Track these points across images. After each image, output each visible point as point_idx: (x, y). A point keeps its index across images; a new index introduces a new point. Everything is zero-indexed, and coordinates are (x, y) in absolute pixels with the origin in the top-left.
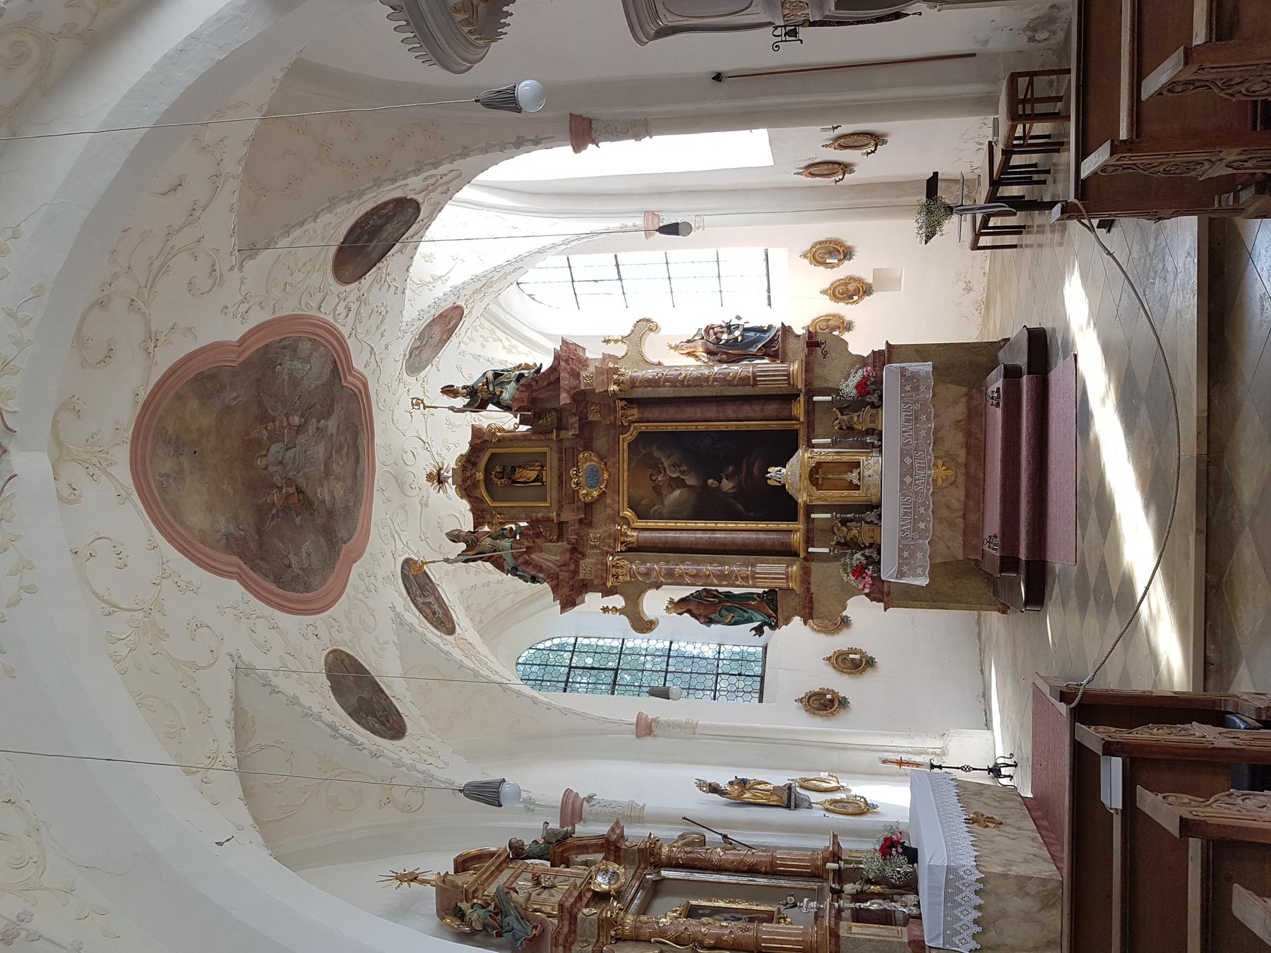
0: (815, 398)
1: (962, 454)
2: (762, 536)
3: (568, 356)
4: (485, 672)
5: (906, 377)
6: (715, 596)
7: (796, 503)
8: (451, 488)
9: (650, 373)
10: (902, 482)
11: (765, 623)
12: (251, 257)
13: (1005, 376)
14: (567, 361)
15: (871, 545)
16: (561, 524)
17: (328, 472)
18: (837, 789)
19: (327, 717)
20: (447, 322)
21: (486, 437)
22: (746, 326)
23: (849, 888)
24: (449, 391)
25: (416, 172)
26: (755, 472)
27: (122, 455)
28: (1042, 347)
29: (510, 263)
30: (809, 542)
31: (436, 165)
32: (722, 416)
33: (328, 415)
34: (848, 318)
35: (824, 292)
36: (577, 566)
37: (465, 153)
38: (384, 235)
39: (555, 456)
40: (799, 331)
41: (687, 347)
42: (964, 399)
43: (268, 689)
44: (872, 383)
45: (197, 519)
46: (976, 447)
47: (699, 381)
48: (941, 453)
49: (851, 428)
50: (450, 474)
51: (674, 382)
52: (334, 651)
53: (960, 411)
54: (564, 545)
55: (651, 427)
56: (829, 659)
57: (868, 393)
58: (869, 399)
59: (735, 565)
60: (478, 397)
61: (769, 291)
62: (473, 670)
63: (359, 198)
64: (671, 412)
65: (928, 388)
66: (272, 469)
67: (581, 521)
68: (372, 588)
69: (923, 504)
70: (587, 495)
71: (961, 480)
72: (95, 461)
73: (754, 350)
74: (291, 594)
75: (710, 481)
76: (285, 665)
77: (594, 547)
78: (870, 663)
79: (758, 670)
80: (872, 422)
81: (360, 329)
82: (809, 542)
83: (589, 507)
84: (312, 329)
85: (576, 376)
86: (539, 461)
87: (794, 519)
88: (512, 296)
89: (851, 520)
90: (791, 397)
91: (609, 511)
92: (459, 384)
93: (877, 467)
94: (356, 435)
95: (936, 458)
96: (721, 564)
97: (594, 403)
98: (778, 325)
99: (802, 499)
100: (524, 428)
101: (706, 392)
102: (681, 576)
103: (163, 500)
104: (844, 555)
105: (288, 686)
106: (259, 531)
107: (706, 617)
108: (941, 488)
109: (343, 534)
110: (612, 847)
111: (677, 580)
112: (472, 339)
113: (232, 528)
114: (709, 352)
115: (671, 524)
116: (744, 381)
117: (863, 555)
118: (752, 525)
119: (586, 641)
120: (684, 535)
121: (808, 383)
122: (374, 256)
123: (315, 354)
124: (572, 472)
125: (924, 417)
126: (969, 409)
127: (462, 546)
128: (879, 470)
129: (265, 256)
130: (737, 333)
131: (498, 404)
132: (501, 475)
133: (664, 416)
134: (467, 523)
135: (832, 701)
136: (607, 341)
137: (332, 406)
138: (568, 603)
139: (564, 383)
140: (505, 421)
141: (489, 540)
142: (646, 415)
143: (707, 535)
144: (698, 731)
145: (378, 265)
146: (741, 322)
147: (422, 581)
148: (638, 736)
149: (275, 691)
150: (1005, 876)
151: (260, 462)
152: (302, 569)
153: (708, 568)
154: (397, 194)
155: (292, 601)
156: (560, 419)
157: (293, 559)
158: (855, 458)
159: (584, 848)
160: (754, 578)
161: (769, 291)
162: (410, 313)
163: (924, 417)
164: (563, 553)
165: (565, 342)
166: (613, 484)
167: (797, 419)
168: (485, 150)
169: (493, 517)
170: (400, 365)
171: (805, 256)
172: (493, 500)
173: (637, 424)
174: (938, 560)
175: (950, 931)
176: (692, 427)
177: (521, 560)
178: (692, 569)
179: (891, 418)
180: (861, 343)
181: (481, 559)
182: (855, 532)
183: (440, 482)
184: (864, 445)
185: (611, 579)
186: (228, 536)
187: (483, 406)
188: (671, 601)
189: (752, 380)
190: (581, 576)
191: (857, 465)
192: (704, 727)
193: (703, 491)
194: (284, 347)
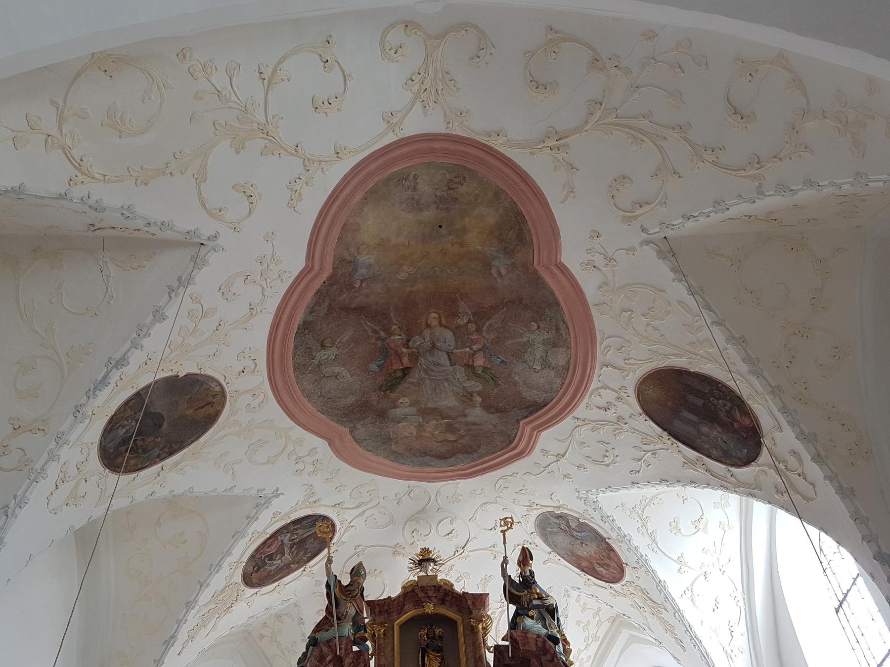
4: (193, 618)
12: (660, 254)
17: (426, 413)
19: (136, 358)
20: (602, 561)
21: (475, 612)
24: (526, 557)
25: (802, 436)
27: (434, 124)
29: (688, 629)
31: (818, 458)
38: (705, 429)
43: (175, 284)
50: (430, 573)
52: (223, 393)
60: (522, 592)
62: (195, 601)
63: (752, 372)
66: (427, 333)
68: (301, 466)
72: (427, 85)
76: (204, 315)
84: (580, 361)
92: (536, 566)
100: (490, 657)
103: (389, 179)
106: (360, 310)
113: (362, 271)
122: (678, 425)
123: (553, 373)
129: (663, 271)
131: (517, 614)
132: (432, 637)
137: (498, 410)
141: (352, 612)
145: (665, 434)
149: (171, 291)
152: (319, 365)
154: (765, 421)
157: (331, 353)
169: (382, 624)
170: (547, 504)
181: (330, 603)
194: (558, 329)
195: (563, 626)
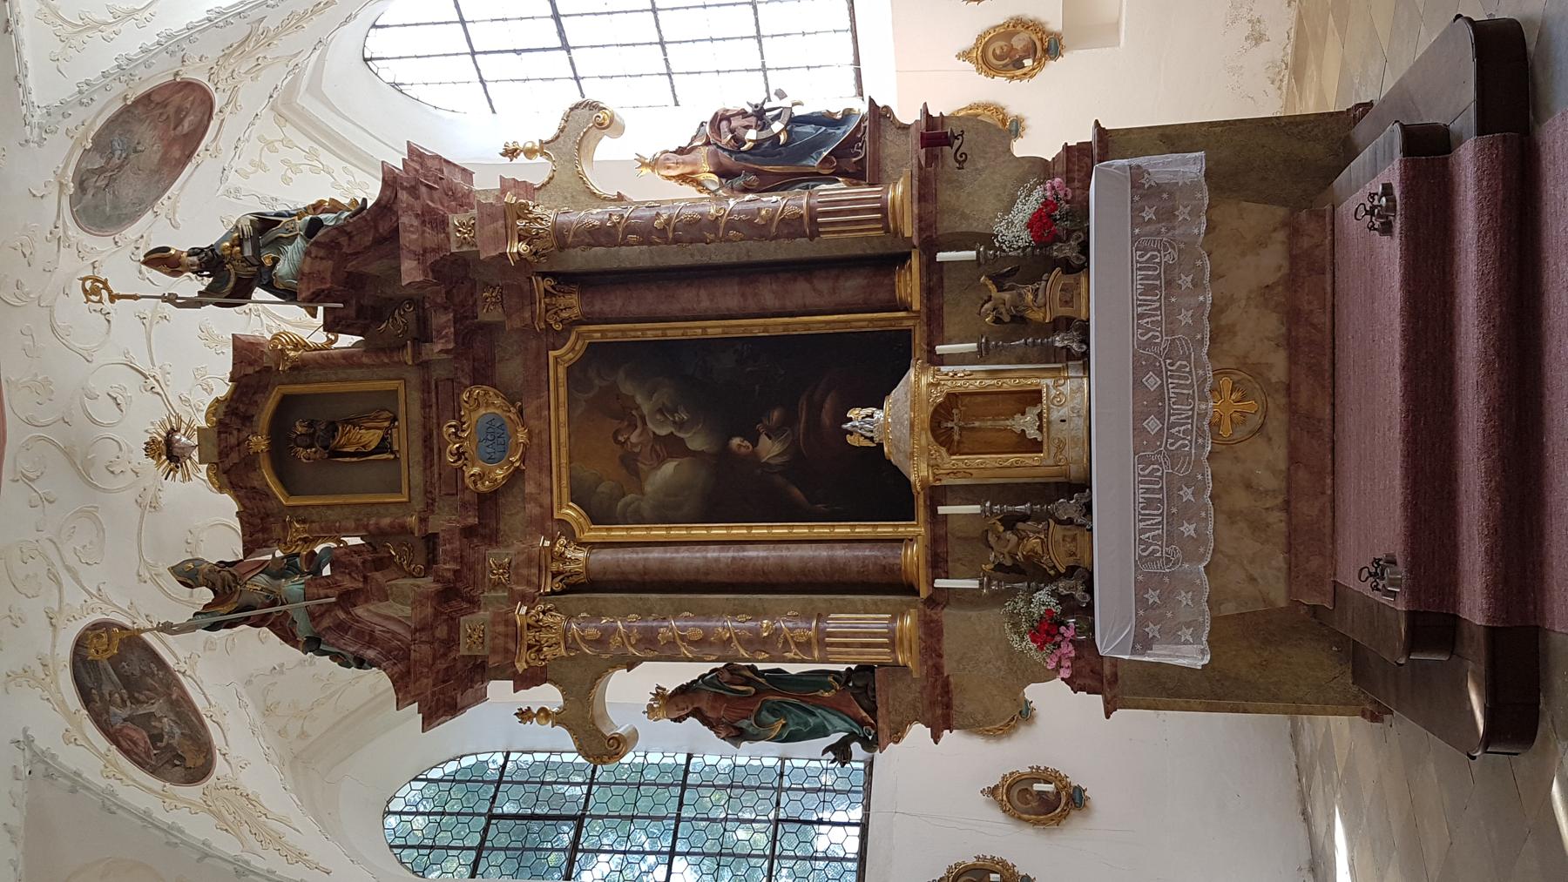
0: (942, 256)
1: (1278, 365)
2: (840, 553)
5: (1143, 190)
6: (748, 682)
9: (595, 215)
10: (1139, 431)
11: (852, 737)
14: (413, 190)
15: (1071, 571)
16: (431, 540)
21: (266, 362)
22: (798, 111)
24: (161, 260)
26: (826, 418)
30: (938, 564)
32: (752, 305)
34: (1013, 110)
35: (965, 55)
36: (454, 629)
39: (416, 396)
40: (908, 114)
42: (1281, 236)
44: (1064, 217)
47: (694, 229)
48: (1229, 363)
49: (1019, 320)
51: (646, 233)
53: (1271, 262)
54: (428, 584)
56: (993, 792)
57: (1056, 238)
58: (1058, 251)
59: (785, 617)
60: (231, 271)
61: (857, 61)
62: (235, 861)
64: (648, 299)
65: (1195, 213)
67: (468, 532)
69: (1189, 481)
70: (481, 476)
71: (1278, 422)
73: (814, 163)
75: (736, 441)
77: (496, 585)
80: (1066, 303)
82: (938, 564)
83: (489, 502)
86: (382, 407)
87: (909, 516)
89: (1024, 518)
90: (889, 262)
91: (532, 509)
92: (180, 244)
93: (1079, 401)
95: (1218, 373)
96: (757, 615)
97: (487, 285)
99: (918, 472)
100: (346, 341)
101: (718, 254)
102: (671, 643)
104: (1013, 593)
107: (731, 725)
108: (1229, 444)
111: (669, 652)
114: (724, 173)
115: (659, 532)
116: (791, 226)
117: (1054, 594)
118: (822, 530)
120: (683, 555)
125: (1186, 281)
126: (1293, 259)
128: (1087, 407)
130: (777, 127)
131: (270, 287)
132: (310, 440)
133: (633, 308)
138: (439, 708)
139: (409, 238)
140: (303, 326)
141: (262, 580)
142: (598, 306)
143: (729, 554)
146: (786, 103)
153: (728, 625)
158: (1031, 383)
160: (823, 645)
163: (1186, 281)
164: (417, 603)
165: (414, 153)
166: (537, 452)
167: (907, 308)
169: (286, 527)
172: (291, 491)
174: (1229, 609)
176: (695, 330)
177: (327, 622)
178: (693, 626)
179: (1109, 293)
180: (1042, 141)
181: (246, 620)
182: (1034, 542)
183: (171, 457)
185: (525, 655)
188: (659, 694)
190: (463, 651)
191: (1034, 397)
193: (722, 460)
195: (291, 208)
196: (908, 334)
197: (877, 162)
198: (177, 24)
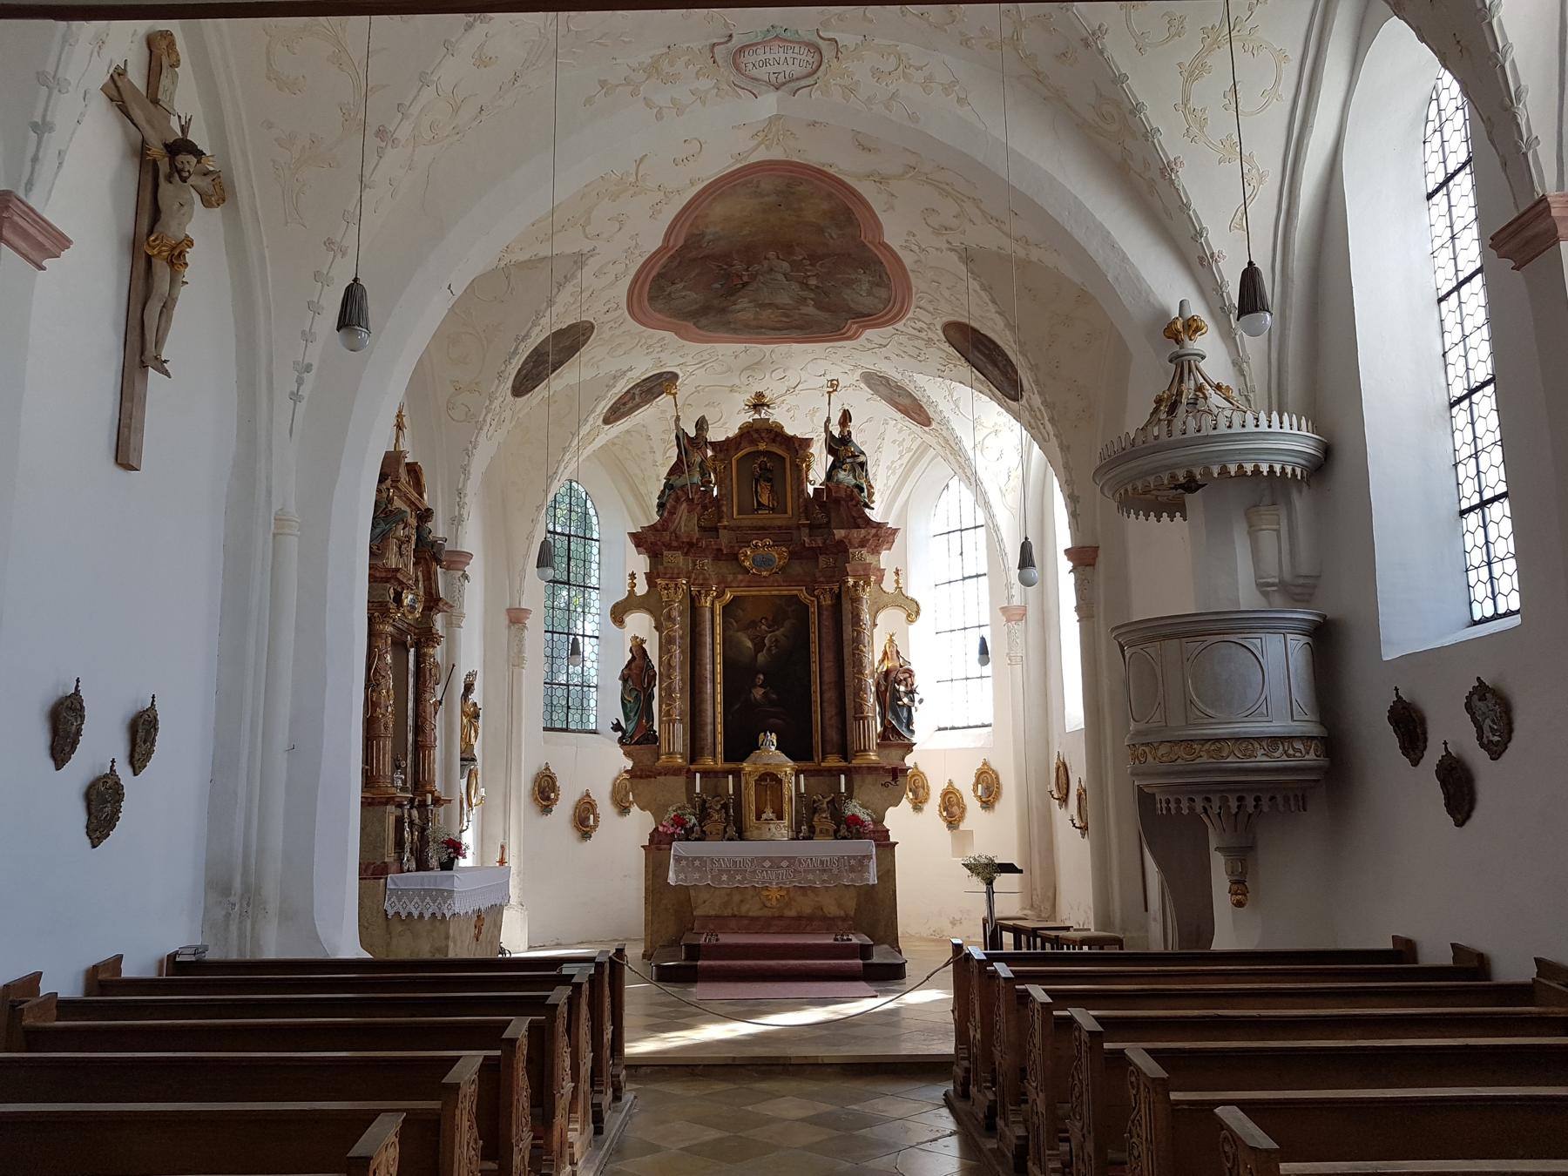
1: (793, 913)
2: (709, 728)
3: (882, 536)
5: (862, 860)
7: (742, 760)
8: (749, 417)
9: (866, 617)
10: (764, 859)
11: (624, 732)
13: (862, 945)
14: (876, 535)
15: (703, 832)
17: (762, 306)
18: (470, 805)
20: (916, 412)
23: (415, 813)
24: (846, 418)
27: (777, 154)
28: (890, 975)
30: (706, 774)
31: (1052, 420)
33: (818, 306)
34: (926, 807)
35: (951, 783)
37: (1064, 448)
39: (784, 523)
40: (909, 761)
41: (892, 651)
45: (719, 210)
46: (801, 923)
47: (859, 665)
49: (815, 811)
51: (857, 641)
53: (832, 909)
54: (696, 535)
55: (814, 618)
59: (680, 704)
60: (840, 447)
61: (953, 728)
64: (829, 638)
66: (766, 263)
69: (744, 878)
73: (889, 716)
74: (647, 288)
77: (694, 563)
78: (586, 835)
79: (572, 727)
81: (902, 339)
82: (706, 774)
83: (734, 557)
84: (899, 299)
85: (863, 544)
86: (778, 508)
87: (726, 760)
88: (943, 469)
89: (727, 813)
91: (730, 577)
92: (853, 427)
94: (800, 328)
98: (914, 740)
99: (746, 766)
101: (848, 671)
102: (669, 651)
105: (564, 298)
106: (707, 257)
109: (704, 322)
110: (433, 602)
112: (901, 431)
114: (887, 673)
115: (718, 639)
116: (859, 708)
119: (595, 551)
120: (708, 653)
121: (858, 769)
122: (971, 357)
124: (768, 541)
126: (833, 919)
127: (692, 433)
128: (776, 837)
130: (906, 700)
131: (833, 466)
132: (762, 467)
133: (824, 630)
134: (716, 434)
135: (548, 798)
136: (897, 573)
137: (828, 310)
138: (639, 540)
139: (855, 532)
140: (817, 474)
141: (698, 459)
142: (825, 614)
143: (709, 675)
144: (516, 670)
147: (656, 390)
148: (509, 611)
150: (447, 937)
151: (771, 254)
153: (677, 676)
155: (640, 295)
156: (819, 527)
159: (429, 578)
161: (953, 728)
162: (921, 380)
166: (757, 581)
168: (1066, 466)
171: (985, 764)
172: (738, 461)
173: (817, 604)
174: (692, 893)
175: (401, 894)
176: (815, 657)
178: (676, 661)
179: (825, 848)
180: (898, 819)
184: (799, 824)
186: (703, 235)
187: (831, 451)
188: (643, 641)
189: (860, 715)
191: (780, 817)
192: (520, 674)
195: (870, 476)
196: (811, 759)
197: (890, 746)
198: (953, 424)
